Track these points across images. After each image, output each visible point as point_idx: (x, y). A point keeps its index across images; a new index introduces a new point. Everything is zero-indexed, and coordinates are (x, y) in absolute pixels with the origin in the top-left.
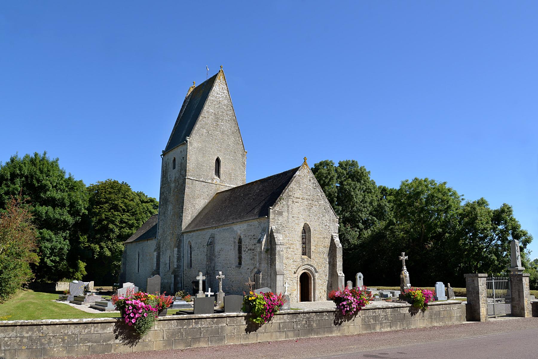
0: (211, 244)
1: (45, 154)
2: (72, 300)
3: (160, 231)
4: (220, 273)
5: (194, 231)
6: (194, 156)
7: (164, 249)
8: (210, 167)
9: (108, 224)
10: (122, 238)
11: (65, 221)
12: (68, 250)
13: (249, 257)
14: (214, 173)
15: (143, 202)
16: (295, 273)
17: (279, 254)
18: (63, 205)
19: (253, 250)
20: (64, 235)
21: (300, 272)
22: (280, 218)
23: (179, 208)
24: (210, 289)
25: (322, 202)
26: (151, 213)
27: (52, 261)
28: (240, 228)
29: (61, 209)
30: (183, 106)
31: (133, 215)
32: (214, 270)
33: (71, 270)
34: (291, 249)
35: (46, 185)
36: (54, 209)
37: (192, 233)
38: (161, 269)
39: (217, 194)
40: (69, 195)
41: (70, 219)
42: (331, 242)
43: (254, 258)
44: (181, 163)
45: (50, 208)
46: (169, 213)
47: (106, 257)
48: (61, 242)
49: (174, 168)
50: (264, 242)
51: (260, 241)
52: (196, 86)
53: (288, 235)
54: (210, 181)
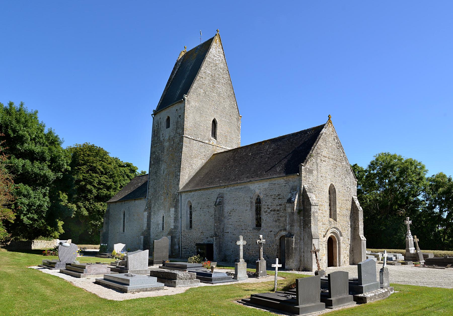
0: (219, 204)
1: (22, 105)
2: (64, 268)
3: (150, 191)
4: (261, 236)
5: (196, 190)
6: (191, 115)
7: (156, 209)
8: (207, 127)
9: (86, 185)
10: (99, 198)
11: (45, 176)
12: (48, 207)
13: (272, 219)
14: (211, 133)
15: (120, 166)
16: (324, 236)
17: (314, 216)
18: (42, 159)
19: (278, 211)
20: (44, 191)
21: (329, 235)
22: (311, 177)
23: (175, 167)
24: (277, 259)
25: (345, 163)
26: (128, 176)
27: (28, 218)
28: (259, 187)
29: (40, 163)
30: (174, 69)
31: (110, 178)
32: (223, 231)
33: (49, 228)
34: (321, 211)
35: (23, 136)
36: (32, 162)
37: (193, 193)
38: (151, 229)
39: (214, 155)
40: (50, 149)
41: (51, 175)
42: (352, 205)
43: (279, 220)
44: (177, 122)
45: (28, 162)
46: (162, 172)
47: (83, 216)
48: (40, 198)
49: (168, 126)
50: (296, 202)
51: (290, 201)
52: (187, 50)
53: (318, 195)
54: (207, 142)
